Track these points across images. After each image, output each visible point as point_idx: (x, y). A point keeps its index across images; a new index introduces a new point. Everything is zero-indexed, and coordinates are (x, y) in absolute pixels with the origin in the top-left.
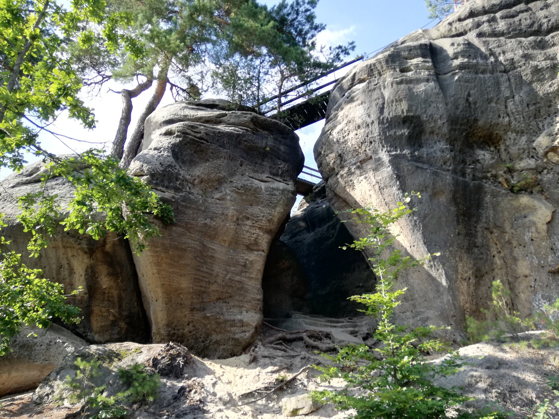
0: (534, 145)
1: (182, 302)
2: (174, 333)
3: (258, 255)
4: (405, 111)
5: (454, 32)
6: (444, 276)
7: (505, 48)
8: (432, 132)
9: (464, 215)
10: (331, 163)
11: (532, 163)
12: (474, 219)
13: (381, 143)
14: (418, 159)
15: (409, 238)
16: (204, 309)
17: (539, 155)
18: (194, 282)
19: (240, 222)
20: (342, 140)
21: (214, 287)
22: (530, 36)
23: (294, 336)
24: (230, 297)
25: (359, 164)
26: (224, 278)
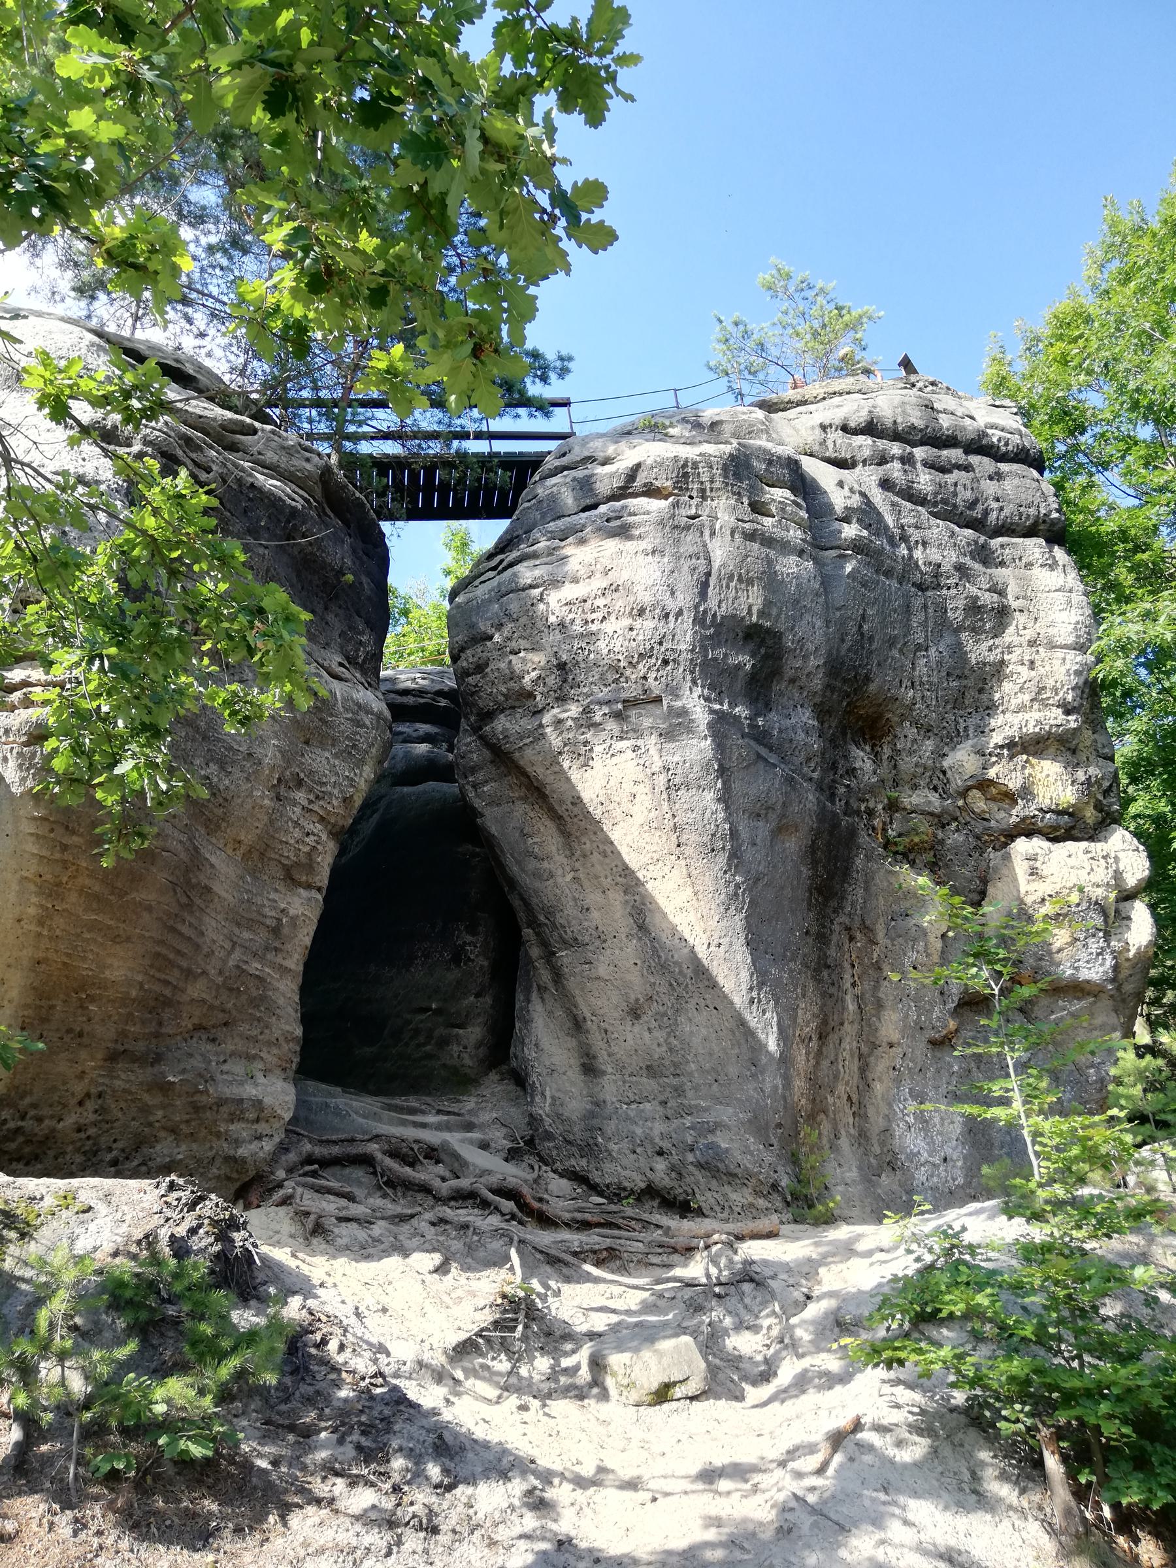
0: (946, 763)
1: (87, 1028)
2: (18, 1130)
3: (309, 899)
4: (755, 610)
5: (830, 454)
6: (775, 1029)
7: (927, 534)
8: (793, 681)
9: (820, 892)
10: (527, 678)
11: (934, 801)
12: (833, 903)
13: (692, 672)
14: (760, 736)
15: (713, 923)
16: (158, 1059)
17: (952, 788)
18: (151, 966)
19: (282, 790)
20: (577, 628)
21: (196, 990)
22: (967, 527)
23: (336, 1150)
24: (226, 1024)
25: (620, 706)
26: (225, 962)
